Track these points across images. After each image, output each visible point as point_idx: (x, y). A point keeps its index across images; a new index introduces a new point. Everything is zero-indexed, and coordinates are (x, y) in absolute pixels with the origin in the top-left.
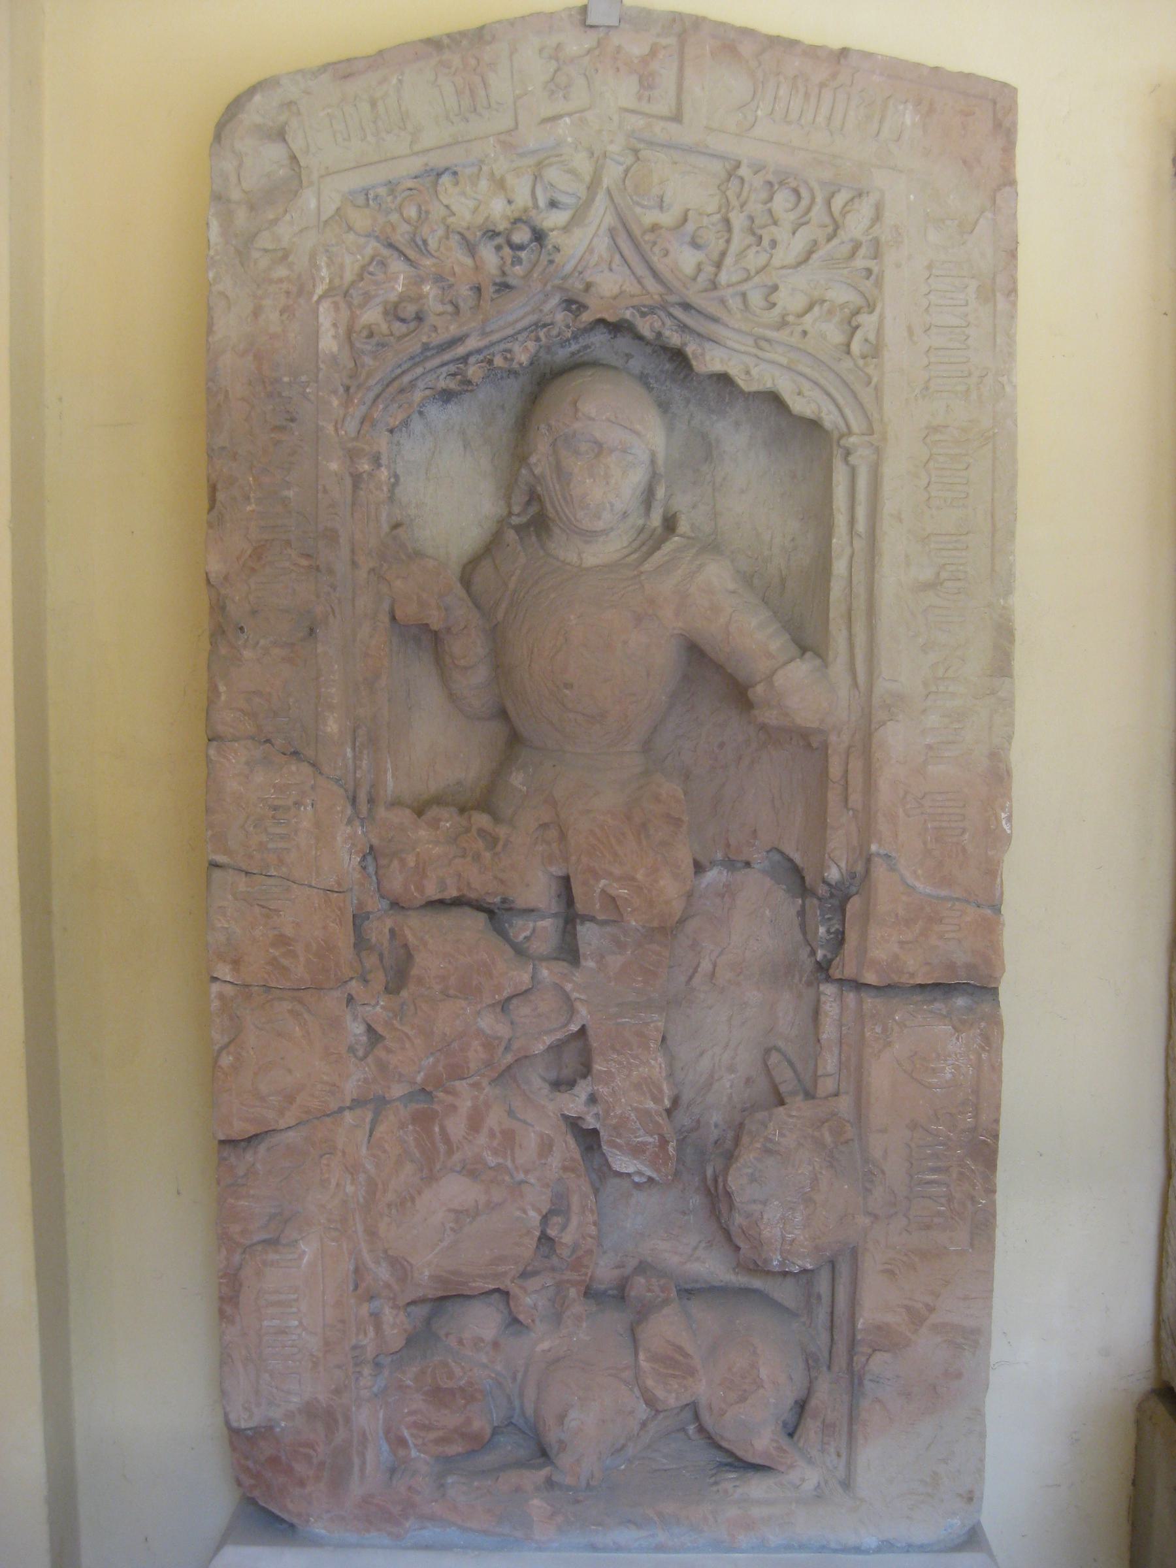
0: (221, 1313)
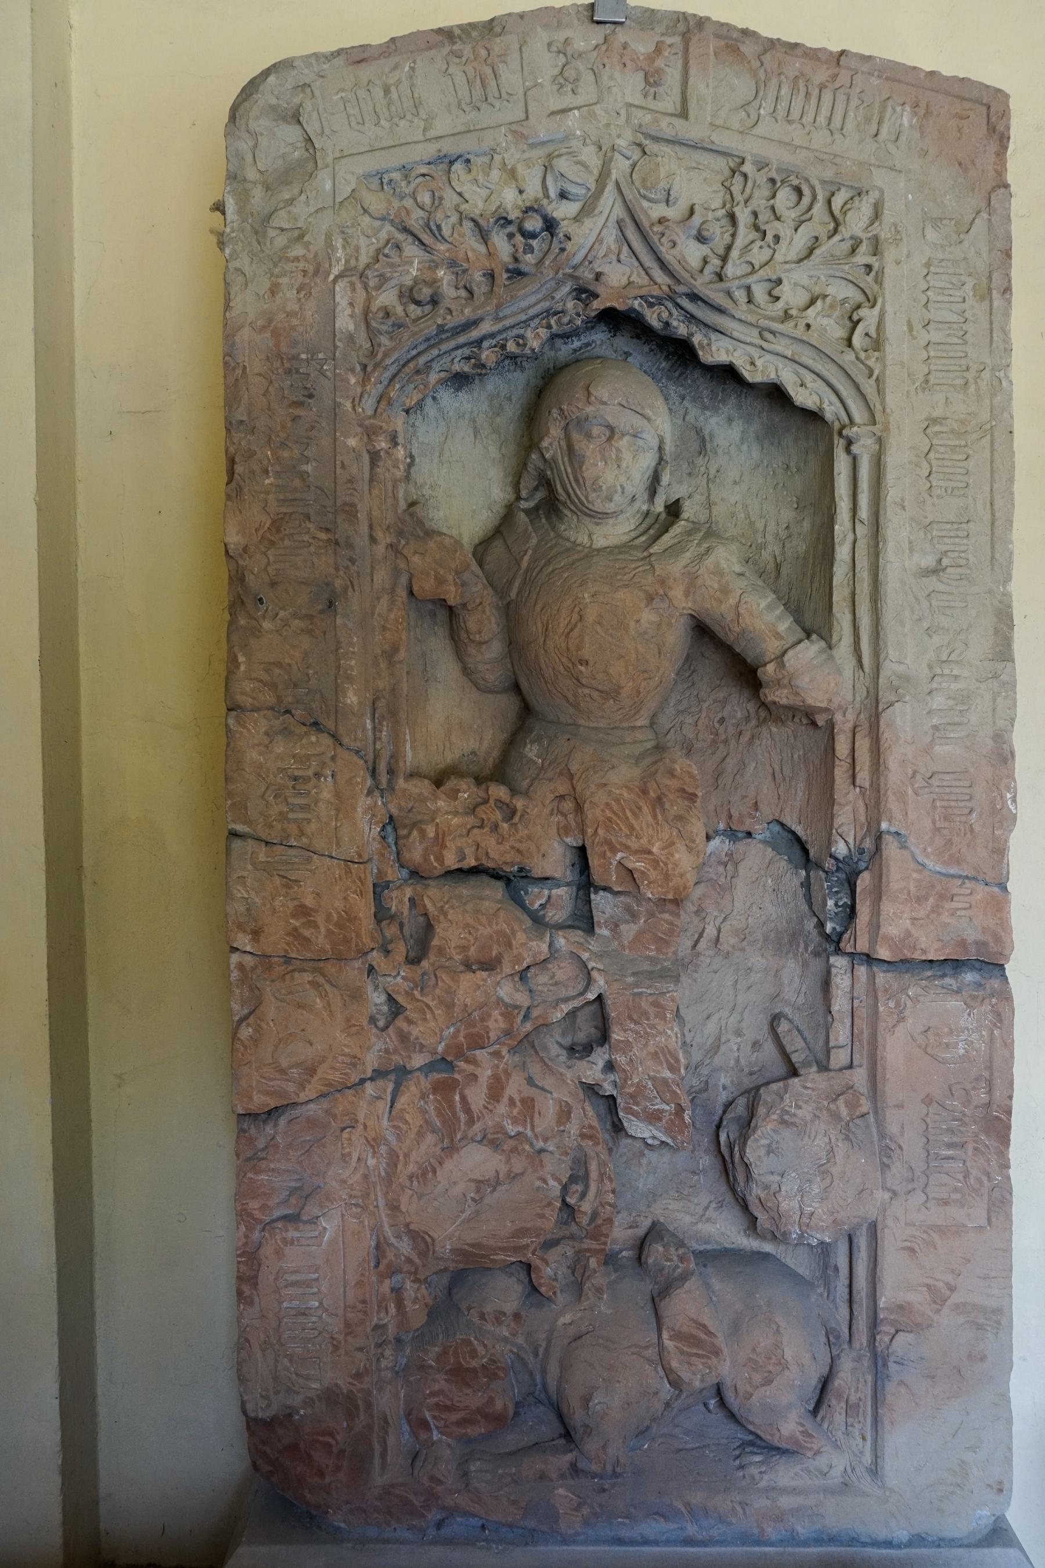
0: (240, 1293)
